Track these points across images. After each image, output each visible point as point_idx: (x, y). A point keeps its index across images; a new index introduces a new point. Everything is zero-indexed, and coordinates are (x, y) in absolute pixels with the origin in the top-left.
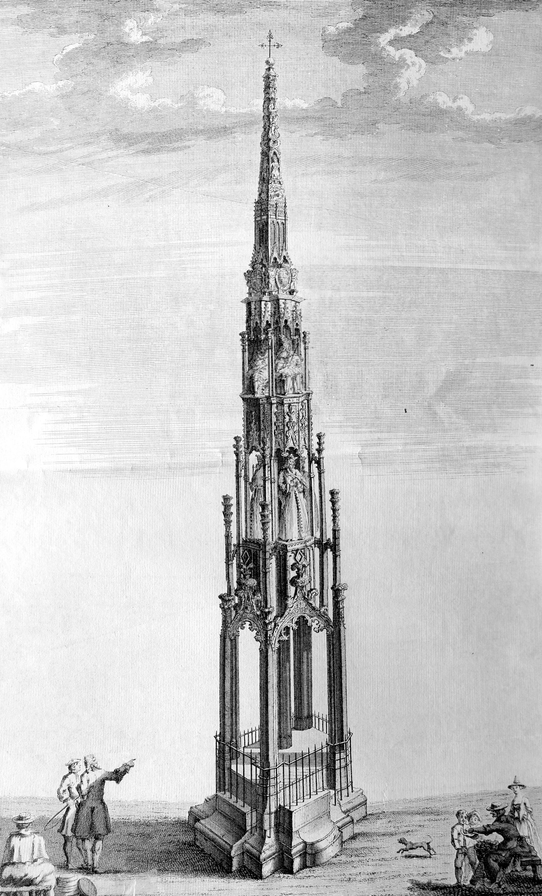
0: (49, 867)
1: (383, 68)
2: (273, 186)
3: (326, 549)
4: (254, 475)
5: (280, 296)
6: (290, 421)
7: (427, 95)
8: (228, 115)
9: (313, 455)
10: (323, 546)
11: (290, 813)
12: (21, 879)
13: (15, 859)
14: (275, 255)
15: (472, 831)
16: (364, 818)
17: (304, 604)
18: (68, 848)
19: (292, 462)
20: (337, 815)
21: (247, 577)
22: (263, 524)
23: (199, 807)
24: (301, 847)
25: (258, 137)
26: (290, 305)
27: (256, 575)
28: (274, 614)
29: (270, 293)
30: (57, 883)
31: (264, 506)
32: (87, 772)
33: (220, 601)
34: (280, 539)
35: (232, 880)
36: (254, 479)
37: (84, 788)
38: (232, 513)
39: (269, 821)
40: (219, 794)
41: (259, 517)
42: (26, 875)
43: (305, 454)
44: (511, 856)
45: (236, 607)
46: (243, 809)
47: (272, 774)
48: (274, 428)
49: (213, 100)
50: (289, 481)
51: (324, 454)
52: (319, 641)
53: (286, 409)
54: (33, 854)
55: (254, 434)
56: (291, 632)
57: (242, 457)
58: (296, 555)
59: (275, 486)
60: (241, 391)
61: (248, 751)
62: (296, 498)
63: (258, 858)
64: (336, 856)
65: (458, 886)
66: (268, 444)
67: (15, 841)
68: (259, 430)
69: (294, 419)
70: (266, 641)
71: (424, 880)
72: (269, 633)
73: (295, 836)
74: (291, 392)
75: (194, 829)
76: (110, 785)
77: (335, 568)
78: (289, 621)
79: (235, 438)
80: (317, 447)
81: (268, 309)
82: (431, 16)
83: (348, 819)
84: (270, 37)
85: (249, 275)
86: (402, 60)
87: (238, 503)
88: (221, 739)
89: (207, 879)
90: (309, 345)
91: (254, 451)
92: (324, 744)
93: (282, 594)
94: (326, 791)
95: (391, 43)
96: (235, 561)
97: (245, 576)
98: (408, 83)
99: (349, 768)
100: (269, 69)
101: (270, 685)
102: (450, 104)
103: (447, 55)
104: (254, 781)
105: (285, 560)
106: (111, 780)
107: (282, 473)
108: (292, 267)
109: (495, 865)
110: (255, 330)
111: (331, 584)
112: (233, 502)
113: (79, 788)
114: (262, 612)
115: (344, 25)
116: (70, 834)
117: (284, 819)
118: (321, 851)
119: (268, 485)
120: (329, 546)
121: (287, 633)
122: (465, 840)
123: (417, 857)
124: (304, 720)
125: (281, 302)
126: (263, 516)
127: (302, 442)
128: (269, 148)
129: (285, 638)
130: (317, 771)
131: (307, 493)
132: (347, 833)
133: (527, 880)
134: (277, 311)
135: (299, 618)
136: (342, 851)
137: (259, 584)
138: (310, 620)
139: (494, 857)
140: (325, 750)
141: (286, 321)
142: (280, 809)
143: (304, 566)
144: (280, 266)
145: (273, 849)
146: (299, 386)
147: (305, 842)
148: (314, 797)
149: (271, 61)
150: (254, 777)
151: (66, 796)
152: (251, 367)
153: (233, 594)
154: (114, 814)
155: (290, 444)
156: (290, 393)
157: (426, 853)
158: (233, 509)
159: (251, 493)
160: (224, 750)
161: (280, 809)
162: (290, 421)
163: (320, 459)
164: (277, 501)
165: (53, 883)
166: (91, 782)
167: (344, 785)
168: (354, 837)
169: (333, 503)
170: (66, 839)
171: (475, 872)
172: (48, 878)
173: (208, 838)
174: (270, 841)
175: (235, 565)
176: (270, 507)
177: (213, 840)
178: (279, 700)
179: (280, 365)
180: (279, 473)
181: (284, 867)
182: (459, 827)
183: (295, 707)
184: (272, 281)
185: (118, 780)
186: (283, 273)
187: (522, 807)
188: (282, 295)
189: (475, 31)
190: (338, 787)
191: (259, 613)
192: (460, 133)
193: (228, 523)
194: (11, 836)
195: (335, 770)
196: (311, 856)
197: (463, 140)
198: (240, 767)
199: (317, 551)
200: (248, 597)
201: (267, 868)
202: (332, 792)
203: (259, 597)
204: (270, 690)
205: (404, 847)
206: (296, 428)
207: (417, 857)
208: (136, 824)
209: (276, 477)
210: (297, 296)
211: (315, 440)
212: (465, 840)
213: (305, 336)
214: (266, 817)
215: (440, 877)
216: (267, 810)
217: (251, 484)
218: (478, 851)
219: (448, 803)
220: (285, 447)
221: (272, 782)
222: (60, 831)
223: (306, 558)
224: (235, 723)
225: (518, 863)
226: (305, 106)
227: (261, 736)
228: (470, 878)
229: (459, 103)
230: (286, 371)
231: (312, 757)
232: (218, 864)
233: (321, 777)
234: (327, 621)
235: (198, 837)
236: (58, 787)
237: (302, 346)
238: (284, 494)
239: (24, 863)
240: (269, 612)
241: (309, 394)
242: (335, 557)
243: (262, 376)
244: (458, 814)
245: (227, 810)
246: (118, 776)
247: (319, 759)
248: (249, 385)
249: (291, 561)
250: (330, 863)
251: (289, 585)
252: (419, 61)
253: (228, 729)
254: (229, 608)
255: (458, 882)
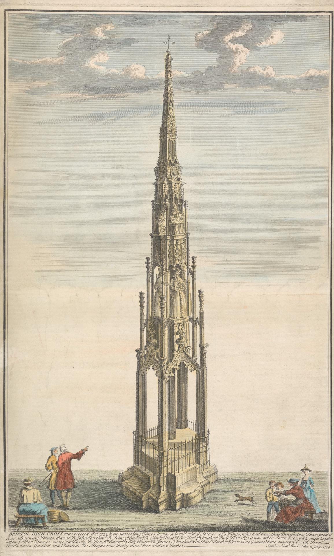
0: (43, 506)
1: (227, 56)
2: (169, 119)
3: (196, 323)
4: (157, 280)
5: (173, 182)
6: (177, 249)
7: (250, 68)
8: (147, 80)
9: (190, 269)
10: (194, 321)
11: (175, 477)
12: (29, 511)
13: (25, 501)
14: (171, 159)
15: (277, 493)
16: (216, 481)
17: (183, 355)
18: (53, 497)
19: (178, 273)
20: (201, 479)
21: (152, 338)
22: (161, 308)
23: (125, 473)
24: (180, 496)
25: (162, 92)
26: (178, 186)
27: (156, 337)
28: (167, 360)
29: (167, 180)
30: (48, 514)
31: (162, 298)
32: (61, 454)
33: (136, 353)
34: (170, 317)
35: (143, 514)
36: (157, 283)
37: (60, 463)
38: (144, 302)
39: (163, 482)
40: (135, 466)
41: (159, 304)
42: (31, 510)
43: (185, 269)
44: (299, 508)
45: (145, 356)
46: (148, 474)
47: (165, 454)
48: (168, 253)
49: (139, 71)
50: (176, 285)
51: (196, 269)
52: (192, 377)
53: (175, 243)
54: (34, 499)
55: (157, 257)
56: (176, 371)
57: (150, 270)
58: (179, 326)
59: (168, 287)
60: (151, 232)
61: (151, 440)
62: (180, 294)
63: (157, 502)
64: (200, 501)
65: (268, 521)
66: (165, 262)
67: (24, 492)
68: (160, 254)
69: (179, 248)
70: (162, 376)
71: (249, 517)
72: (164, 371)
73: (177, 490)
74: (178, 233)
75: (121, 486)
76: (74, 461)
77: (201, 335)
78: (175, 365)
79: (147, 258)
80: (192, 264)
81: (166, 188)
82: (252, 26)
83: (207, 481)
84: (169, 38)
85: (156, 169)
86: (237, 49)
87: (148, 297)
88: (137, 434)
89: (129, 513)
90: (188, 208)
91: (157, 267)
92: (194, 438)
93: (171, 350)
94: (195, 465)
95: (230, 41)
96: (145, 329)
97: (151, 338)
98: (240, 61)
99: (208, 452)
100: (168, 55)
101: (164, 403)
102: (262, 71)
103: (261, 46)
104: (154, 458)
105: (173, 329)
106: (75, 458)
107: (172, 280)
108: (179, 166)
109: (290, 512)
110: (159, 199)
111: (198, 343)
112: (145, 296)
113: (57, 463)
114: (160, 359)
115: (207, 32)
116: (53, 488)
117: (171, 481)
118: (192, 498)
119: (164, 286)
120: (198, 322)
121: (174, 372)
122: (273, 497)
123: (245, 504)
124: (183, 423)
125: (173, 184)
126: (161, 304)
127: (184, 261)
128: (168, 98)
129: (173, 375)
130: (190, 453)
131: (186, 292)
132: (206, 489)
133: (307, 520)
134: (171, 190)
135: (181, 363)
136: (204, 499)
137: (158, 342)
138: (186, 364)
139: (289, 508)
140: (194, 441)
141: (176, 195)
142: (169, 474)
143: (184, 333)
144: (173, 165)
145: (165, 497)
146: (182, 230)
147: (183, 494)
148: (188, 468)
149: (169, 51)
150: (155, 456)
151: (51, 467)
152: (157, 219)
153: (143, 349)
154: (77, 477)
155: (177, 262)
156: (177, 234)
157: (251, 503)
158: (145, 300)
159: (155, 291)
160: (138, 440)
161: (169, 474)
162: (177, 249)
163: (193, 271)
164: (169, 296)
165: (46, 514)
166: (64, 460)
167: (205, 462)
168: (210, 492)
169: (200, 297)
170: (52, 491)
171: (278, 515)
172: (43, 511)
173: (129, 490)
174: (164, 492)
175: (145, 331)
176: (165, 299)
177: (132, 492)
178: (169, 411)
179: (172, 218)
180: (170, 280)
181: (171, 507)
182: (270, 490)
183: (178, 415)
184: (168, 173)
185: (79, 459)
186: (174, 168)
187: (308, 482)
188: (174, 181)
189: (274, 33)
190: (201, 463)
191: (158, 360)
192: (268, 88)
193: (142, 307)
194: (22, 490)
195: (200, 453)
196: (186, 501)
197: (270, 91)
198: (147, 450)
199: (191, 324)
200: (152, 351)
201: (162, 508)
202: (198, 466)
203: (158, 351)
204: (164, 405)
205: (238, 499)
206: (180, 253)
207: (245, 504)
208: (90, 483)
209: (169, 282)
210: (182, 181)
211: (191, 260)
212: (273, 497)
213: (185, 203)
214: (161, 479)
215: (258, 516)
216: (162, 475)
217: (155, 286)
218: (281, 504)
219: (264, 476)
220: (174, 264)
221: (165, 459)
222: (48, 487)
223: (184, 328)
224: (144, 424)
225: (303, 512)
226: (186, 75)
227: (159, 432)
228: (275, 518)
229: (267, 71)
230: (175, 221)
231: (187, 445)
232: (135, 505)
233: (192, 457)
234: (197, 365)
235: (124, 489)
236: (46, 463)
237: (184, 208)
238: (173, 292)
239: (30, 504)
240: (164, 360)
241: (187, 234)
242: (201, 328)
243: (163, 224)
244: (270, 483)
245: (140, 475)
246: (78, 456)
247: (191, 446)
248: (156, 229)
249: (176, 330)
250: (196, 506)
251: (175, 343)
252: (246, 49)
253: (140, 428)
254: (141, 357)
255: (268, 519)
